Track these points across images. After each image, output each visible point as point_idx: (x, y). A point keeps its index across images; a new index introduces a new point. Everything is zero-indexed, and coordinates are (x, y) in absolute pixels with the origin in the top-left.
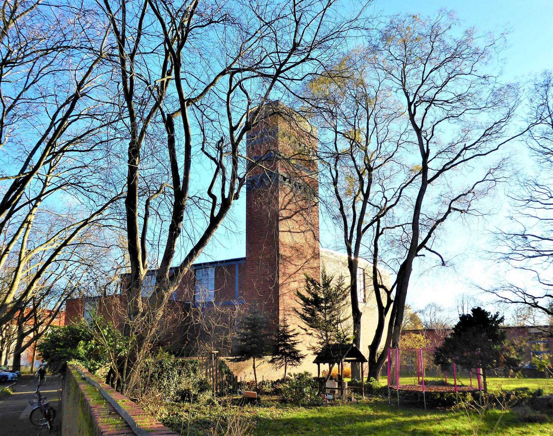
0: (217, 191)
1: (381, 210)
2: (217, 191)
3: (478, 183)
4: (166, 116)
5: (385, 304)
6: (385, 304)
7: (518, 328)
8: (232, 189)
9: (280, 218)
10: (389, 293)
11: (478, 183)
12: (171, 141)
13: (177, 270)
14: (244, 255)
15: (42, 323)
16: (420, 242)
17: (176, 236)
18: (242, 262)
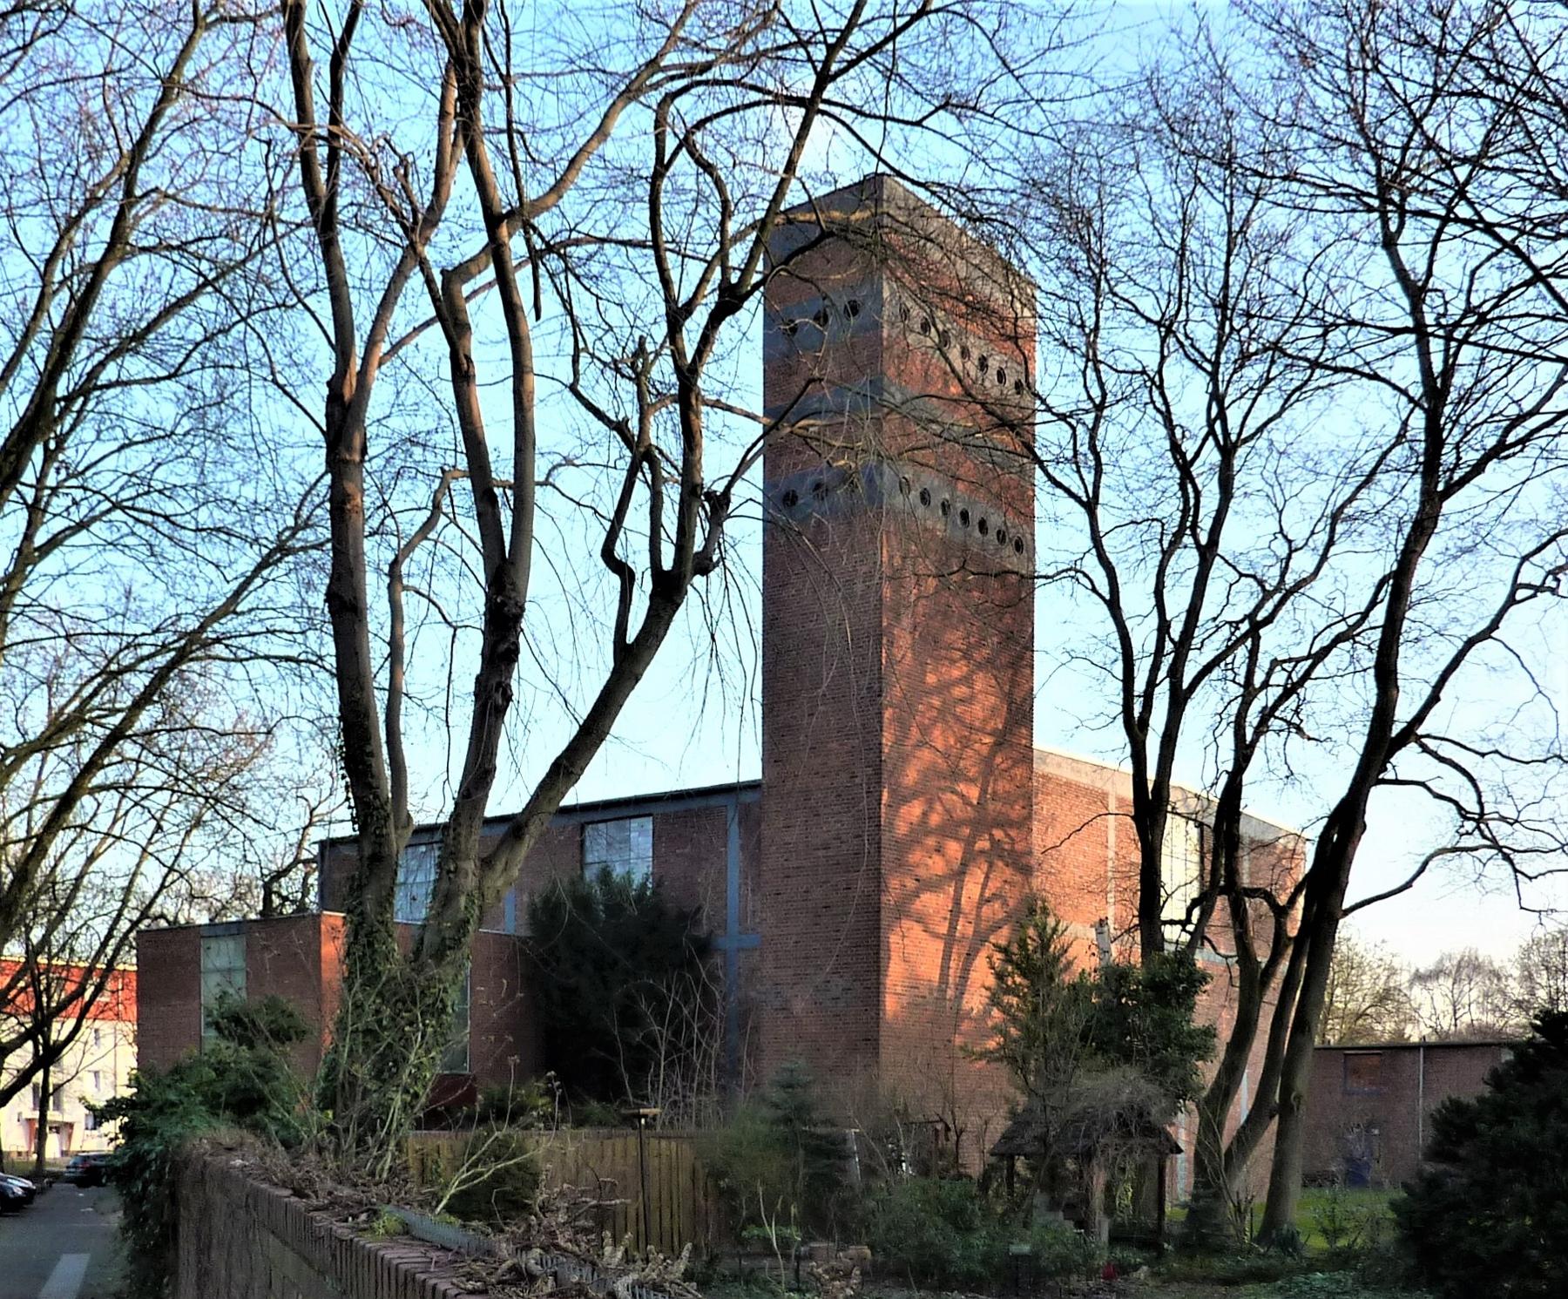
0: (634, 550)
1: (1267, 595)
2: (634, 550)
3: (1408, 885)
4: (438, 279)
5: (1263, 957)
6: (1263, 957)
7: (860, 183)
8: (684, 532)
9: (329, 546)
10: (1281, 913)
11: (1408, 885)
12: (462, 374)
13: (514, 826)
14: (752, 770)
15: (62, 1006)
16: (1309, 662)
17: (500, 711)
18: (748, 797)
